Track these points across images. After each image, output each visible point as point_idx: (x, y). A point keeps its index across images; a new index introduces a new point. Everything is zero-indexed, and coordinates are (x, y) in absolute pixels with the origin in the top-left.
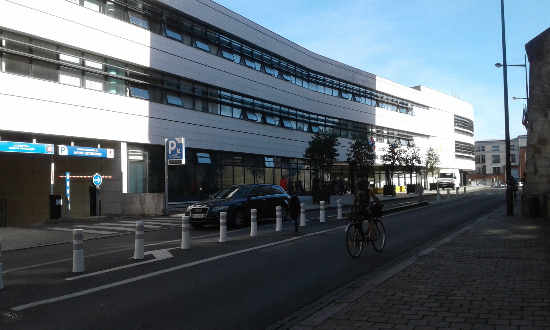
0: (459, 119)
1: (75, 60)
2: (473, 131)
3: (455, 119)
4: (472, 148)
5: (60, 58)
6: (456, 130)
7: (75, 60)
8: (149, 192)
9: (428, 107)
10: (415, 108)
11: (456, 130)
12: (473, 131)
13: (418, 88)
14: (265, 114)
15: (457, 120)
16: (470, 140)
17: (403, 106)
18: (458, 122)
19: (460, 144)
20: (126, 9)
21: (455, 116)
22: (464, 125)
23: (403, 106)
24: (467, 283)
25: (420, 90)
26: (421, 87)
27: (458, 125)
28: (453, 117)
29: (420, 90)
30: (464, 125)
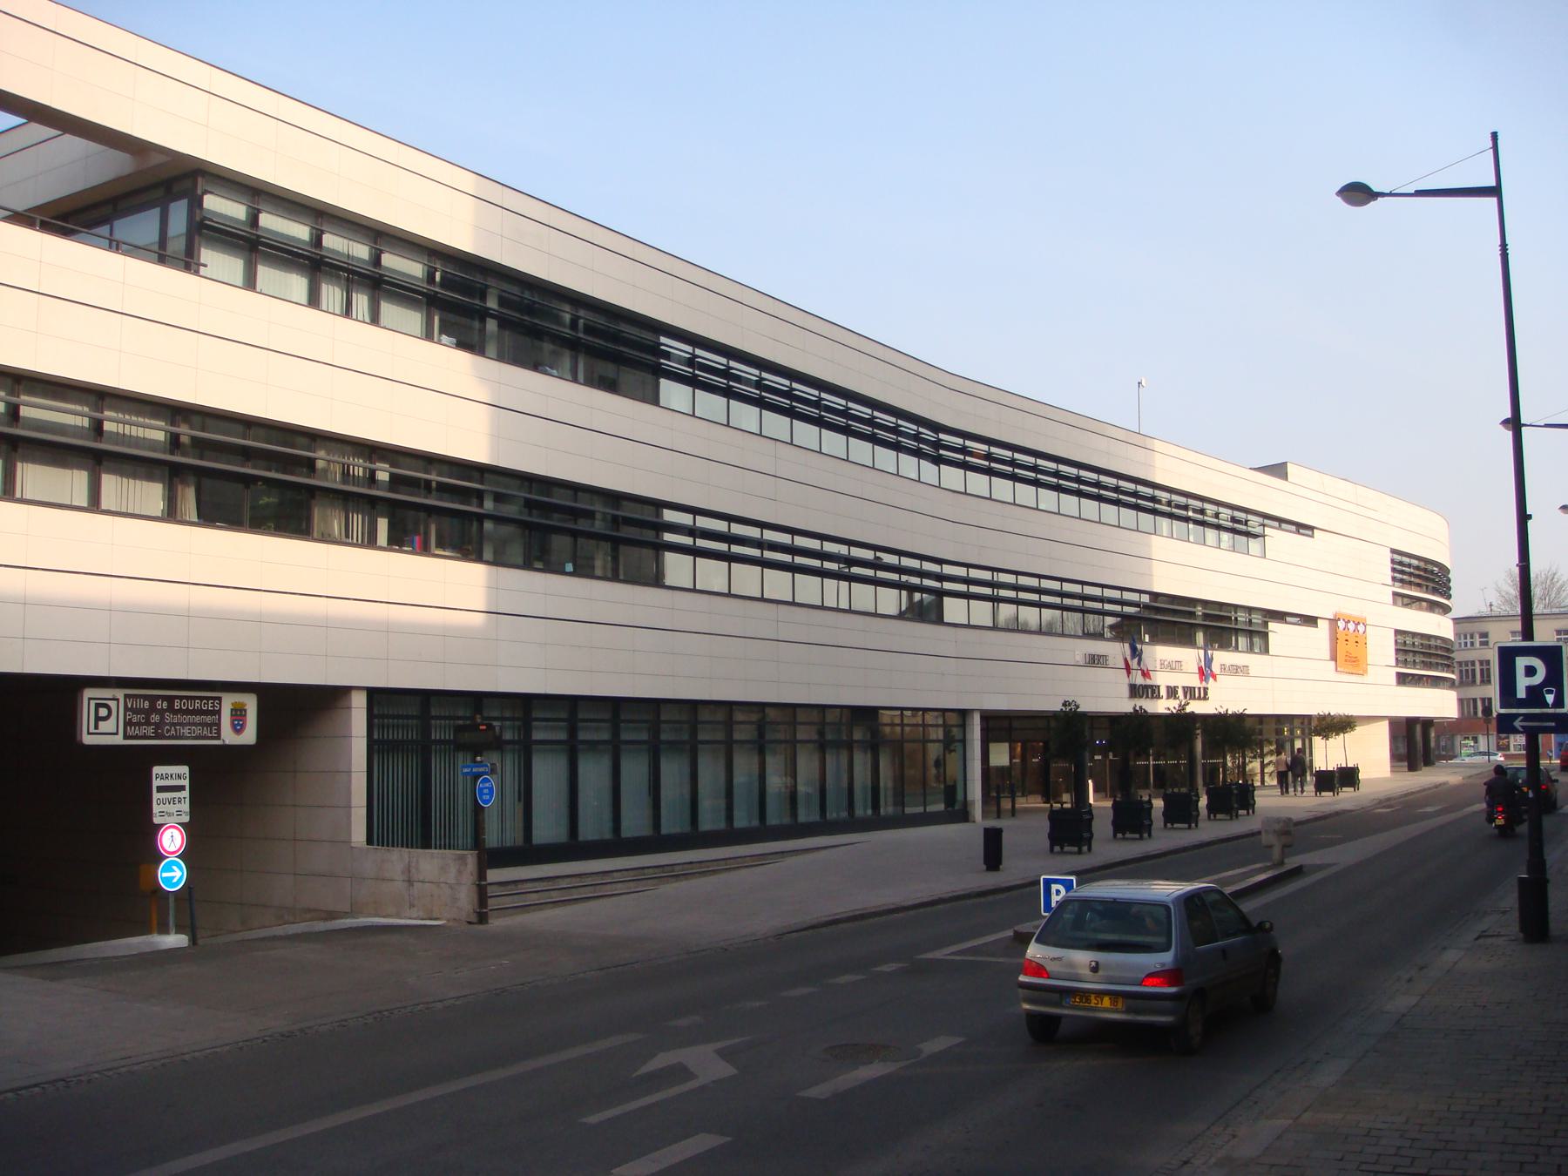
0: (1406, 560)
1: (299, 231)
2: (1449, 597)
3: (1393, 561)
4: (1448, 650)
5: (325, 243)
6: (1395, 594)
7: (299, 231)
8: (986, 830)
9: (1311, 528)
10: (1274, 536)
11: (1395, 594)
12: (1449, 597)
13: (1279, 470)
14: (1169, 665)
15: (1401, 563)
16: (1439, 626)
17: (1240, 525)
18: (1402, 572)
19: (1409, 640)
20: (537, 334)
21: (1394, 551)
22: (1422, 579)
23: (1240, 525)
24: (890, 601)
25: (1284, 476)
26: (1290, 468)
27: (1401, 581)
28: (1389, 555)
29: (1284, 476)
30: (1422, 579)
